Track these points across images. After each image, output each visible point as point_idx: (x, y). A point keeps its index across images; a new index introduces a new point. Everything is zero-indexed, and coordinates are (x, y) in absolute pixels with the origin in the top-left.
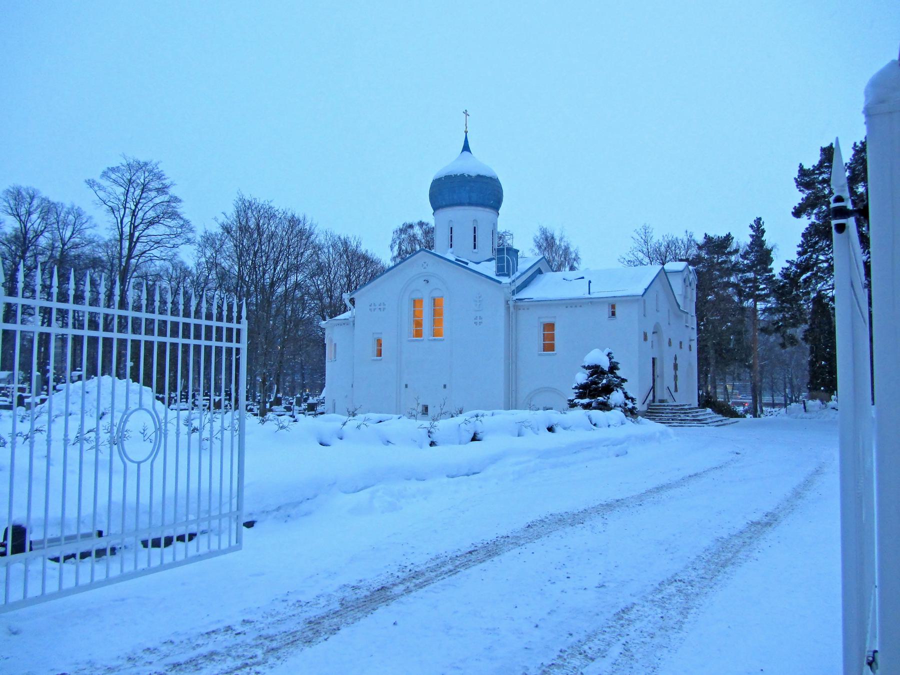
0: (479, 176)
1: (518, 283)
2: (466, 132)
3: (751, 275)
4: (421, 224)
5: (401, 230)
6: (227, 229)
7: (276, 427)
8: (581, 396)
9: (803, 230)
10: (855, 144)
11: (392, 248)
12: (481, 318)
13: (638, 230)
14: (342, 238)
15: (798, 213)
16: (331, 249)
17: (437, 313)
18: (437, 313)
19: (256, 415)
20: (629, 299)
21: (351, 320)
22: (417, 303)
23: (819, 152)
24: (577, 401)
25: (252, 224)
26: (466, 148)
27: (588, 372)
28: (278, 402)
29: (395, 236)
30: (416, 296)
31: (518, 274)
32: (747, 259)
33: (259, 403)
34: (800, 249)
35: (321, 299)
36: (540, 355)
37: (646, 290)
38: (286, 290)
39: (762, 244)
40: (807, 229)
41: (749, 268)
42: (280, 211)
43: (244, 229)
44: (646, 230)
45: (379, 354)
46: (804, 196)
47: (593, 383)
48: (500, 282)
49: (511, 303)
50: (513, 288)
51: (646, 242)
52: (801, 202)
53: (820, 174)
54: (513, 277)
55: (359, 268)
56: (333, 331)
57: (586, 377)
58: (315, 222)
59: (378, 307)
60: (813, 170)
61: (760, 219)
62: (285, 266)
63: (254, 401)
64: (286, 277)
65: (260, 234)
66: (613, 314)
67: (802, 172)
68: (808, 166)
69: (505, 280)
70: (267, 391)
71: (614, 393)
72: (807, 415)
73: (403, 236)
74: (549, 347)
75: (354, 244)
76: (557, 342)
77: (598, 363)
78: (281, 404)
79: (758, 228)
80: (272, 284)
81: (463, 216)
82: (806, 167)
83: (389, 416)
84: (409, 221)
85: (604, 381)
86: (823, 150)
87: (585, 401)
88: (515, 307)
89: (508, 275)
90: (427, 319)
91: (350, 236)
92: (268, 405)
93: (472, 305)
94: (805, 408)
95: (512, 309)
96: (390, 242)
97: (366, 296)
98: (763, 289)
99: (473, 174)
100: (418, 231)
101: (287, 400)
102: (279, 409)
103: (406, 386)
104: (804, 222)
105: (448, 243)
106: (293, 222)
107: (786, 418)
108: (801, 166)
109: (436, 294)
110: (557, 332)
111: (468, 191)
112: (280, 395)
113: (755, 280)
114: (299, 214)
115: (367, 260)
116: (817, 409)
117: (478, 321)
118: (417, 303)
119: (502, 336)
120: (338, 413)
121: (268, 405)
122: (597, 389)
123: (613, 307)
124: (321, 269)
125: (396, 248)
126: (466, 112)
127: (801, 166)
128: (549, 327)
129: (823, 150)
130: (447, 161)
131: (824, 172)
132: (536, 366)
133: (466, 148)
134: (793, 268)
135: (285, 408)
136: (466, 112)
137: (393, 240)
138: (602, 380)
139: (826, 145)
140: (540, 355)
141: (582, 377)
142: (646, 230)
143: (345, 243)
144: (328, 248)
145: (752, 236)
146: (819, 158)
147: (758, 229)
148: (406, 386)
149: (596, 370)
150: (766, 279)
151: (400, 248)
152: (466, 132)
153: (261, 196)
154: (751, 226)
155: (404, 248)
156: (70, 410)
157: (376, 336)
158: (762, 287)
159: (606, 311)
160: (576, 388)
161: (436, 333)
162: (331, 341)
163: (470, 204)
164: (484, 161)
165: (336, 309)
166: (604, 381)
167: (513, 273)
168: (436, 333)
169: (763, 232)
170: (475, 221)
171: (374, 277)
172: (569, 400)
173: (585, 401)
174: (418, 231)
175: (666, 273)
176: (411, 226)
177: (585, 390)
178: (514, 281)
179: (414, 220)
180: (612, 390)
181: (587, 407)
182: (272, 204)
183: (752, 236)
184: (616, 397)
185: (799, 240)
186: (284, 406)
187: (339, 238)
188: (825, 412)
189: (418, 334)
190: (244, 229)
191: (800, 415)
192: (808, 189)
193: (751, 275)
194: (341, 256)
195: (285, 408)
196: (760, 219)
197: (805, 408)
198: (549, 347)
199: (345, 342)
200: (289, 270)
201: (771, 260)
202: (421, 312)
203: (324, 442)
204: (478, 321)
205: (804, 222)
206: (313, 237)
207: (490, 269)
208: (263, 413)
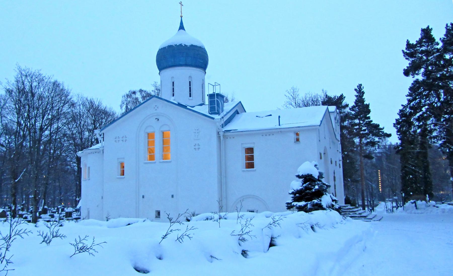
0: (192, 45)
1: (225, 119)
2: (181, 17)
3: (357, 121)
4: (141, 91)
5: (127, 95)
6: (9, 92)
7: (72, 250)
8: (296, 199)
9: (410, 85)
10: (447, 25)
11: (121, 107)
12: (199, 145)
13: (289, 90)
14: (89, 99)
15: (406, 73)
16: (81, 107)
17: (165, 142)
18: (165, 142)
19: (29, 221)
20: (310, 129)
21: (101, 149)
22: (150, 136)
23: (420, 32)
24: (295, 203)
25: (27, 88)
26: (182, 27)
27: (301, 180)
28: (45, 211)
29: (124, 99)
30: (150, 130)
31: (225, 113)
32: (353, 110)
33: (31, 212)
34: (409, 98)
35: (74, 139)
36: (243, 171)
37: (321, 121)
38: (51, 133)
39: (362, 101)
40: (412, 84)
41: (356, 117)
42: (47, 76)
43: (21, 91)
44: (294, 91)
45: (123, 174)
46: (409, 62)
47: (306, 188)
48: (213, 118)
49: (221, 134)
50: (222, 122)
51: (294, 98)
52: (408, 65)
53: (421, 47)
54: (222, 115)
55: (100, 117)
56: (88, 158)
57: (301, 184)
58: (70, 88)
59: (121, 139)
60: (416, 44)
61: (361, 85)
62: (50, 117)
63: (27, 211)
64: (51, 125)
65: (33, 95)
66: (298, 140)
67: (409, 46)
68: (413, 41)
69: (216, 117)
70: (36, 202)
71: (324, 196)
72: (419, 211)
73: (129, 99)
74: (250, 165)
75: (97, 103)
76: (256, 161)
77: (310, 173)
78: (47, 213)
79: (360, 90)
80: (42, 129)
81: (181, 74)
82: (411, 42)
83: (137, 219)
84: (133, 89)
85: (317, 187)
86: (423, 30)
87: (302, 203)
88: (223, 136)
89: (218, 113)
90: (157, 147)
91: (94, 98)
92: (38, 214)
93: (193, 134)
94: (416, 206)
95: (222, 138)
96: (120, 103)
97: (111, 133)
98: (365, 130)
99: (188, 44)
100: (138, 95)
101: (50, 210)
102: (46, 216)
103: (143, 197)
104: (410, 80)
105: (171, 92)
106: (56, 84)
107: (404, 213)
108: (408, 42)
109: (165, 128)
110: (256, 154)
111: (183, 57)
112: (46, 207)
113: (359, 124)
114: (60, 81)
115: (106, 113)
116: (423, 206)
117: (197, 147)
118: (150, 136)
119: (215, 158)
120: (93, 218)
121: (38, 214)
122: (309, 195)
123: (297, 134)
124: (75, 118)
125: (124, 107)
126: (181, 3)
127: (408, 42)
128: (250, 150)
129: (423, 30)
130: (169, 36)
131: (423, 46)
132: (242, 181)
133: (182, 27)
134: (408, 110)
135: (50, 215)
136: (181, 3)
137: (122, 102)
138: (314, 186)
139: (425, 27)
140: (243, 171)
141: (298, 185)
142: (294, 91)
143: (91, 103)
144: (80, 105)
145: (357, 96)
146: (420, 37)
147: (360, 91)
148: (143, 197)
149: (308, 178)
150: (366, 123)
151: (127, 107)
152: (181, 17)
153: (34, 68)
154: (356, 90)
155: (129, 107)
156: (414, 204)
157: (121, 160)
158: (364, 128)
159: (293, 136)
160: (293, 193)
161: (165, 157)
162: (86, 165)
163: (186, 65)
164: (193, 36)
165: (84, 145)
166: (317, 187)
167: (222, 111)
168: (165, 157)
169: (363, 93)
170: (190, 77)
171: (114, 121)
172: (288, 203)
173: (302, 203)
174: (138, 95)
175: (329, 113)
176: (134, 93)
177: (299, 195)
178: (223, 118)
179: (137, 89)
180: (323, 194)
181: (300, 209)
182: (41, 72)
183: (357, 96)
184: (326, 200)
185: (407, 92)
186: (49, 214)
187: (87, 99)
188: (430, 209)
189: (152, 158)
190: (21, 91)
191: (413, 212)
192: (412, 57)
193: (357, 121)
194: (89, 111)
195: (50, 215)
196: (361, 85)
197: (416, 206)
198: (250, 165)
199: (95, 167)
200: (52, 119)
201: (369, 112)
202: (154, 141)
203: (141, 266)
204: (197, 147)
205: (410, 80)
206: (69, 97)
207: (205, 110)
208: (35, 220)
